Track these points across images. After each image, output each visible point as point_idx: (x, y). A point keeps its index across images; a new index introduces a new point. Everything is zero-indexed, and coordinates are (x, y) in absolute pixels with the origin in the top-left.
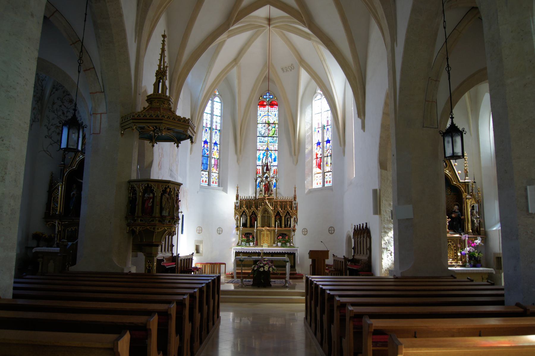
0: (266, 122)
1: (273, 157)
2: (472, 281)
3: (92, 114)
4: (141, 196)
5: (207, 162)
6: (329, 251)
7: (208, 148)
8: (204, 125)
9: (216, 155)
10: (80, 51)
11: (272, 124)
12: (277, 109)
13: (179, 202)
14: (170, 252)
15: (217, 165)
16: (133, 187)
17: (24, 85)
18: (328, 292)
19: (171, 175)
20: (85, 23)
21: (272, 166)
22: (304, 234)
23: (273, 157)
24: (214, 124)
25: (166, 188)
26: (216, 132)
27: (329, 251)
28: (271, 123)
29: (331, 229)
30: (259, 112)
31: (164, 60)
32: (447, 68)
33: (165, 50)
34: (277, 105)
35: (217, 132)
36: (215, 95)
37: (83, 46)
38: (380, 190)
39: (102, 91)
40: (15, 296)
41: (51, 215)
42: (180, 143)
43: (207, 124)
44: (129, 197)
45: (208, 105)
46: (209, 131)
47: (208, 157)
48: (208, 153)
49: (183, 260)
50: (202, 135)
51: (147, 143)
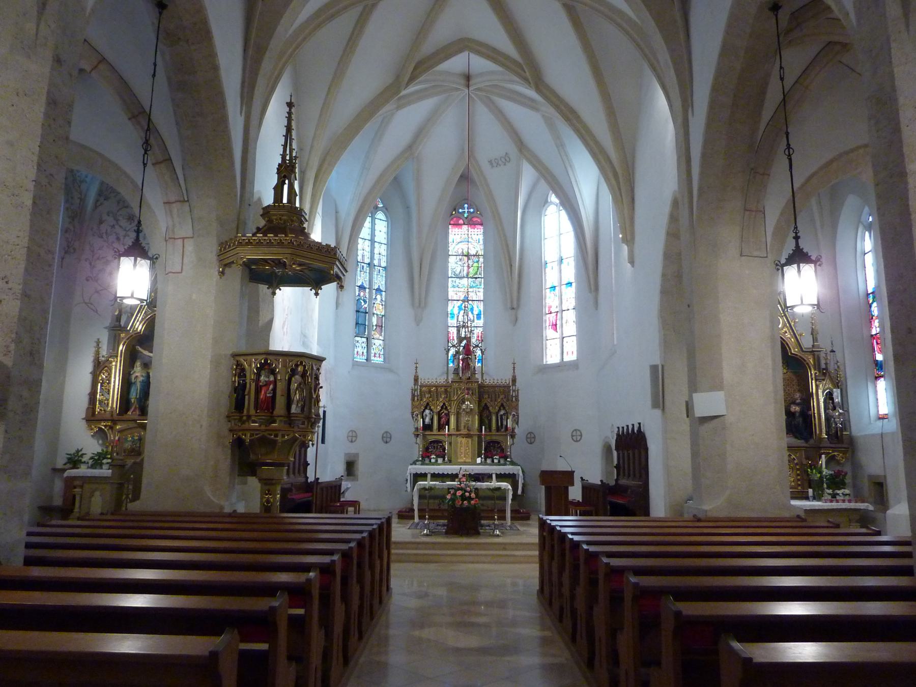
0: (463, 253)
1: (476, 312)
2: (838, 526)
3: (167, 239)
4: (254, 380)
5: (365, 323)
6: (574, 472)
7: (366, 297)
8: (360, 258)
9: (379, 309)
10: (146, 127)
11: (474, 256)
12: (482, 230)
13: (320, 390)
14: (303, 475)
15: (382, 326)
16: (239, 364)
17: (46, 185)
18: (585, 547)
19: (304, 344)
20: (154, 79)
21: (474, 327)
22: (529, 441)
23: (476, 312)
24: (376, 256)
25: (297, 366)
26: (379, 270)
27: (574, 472)
28: (472, 254)
29: (576, 433)
30: (451, 237)
31: (291, 145)
32: (787, 150)
33: (293, 129)
34: (482, 224)
35: (381, 271)
36: (376, 208)
37: (151, 122)
38: (663, 366)
39: (184, 199)
40: (29, 562)
41: (97, 413)
42: (321, 289)
43: (363, 256)
44: (233, 382)
45: (365, 225)
46: (368, 269)
47: (366, 313)
48: (366, 306)
49: (324, 489)
50: (356, 275)
51: (263, 288)
